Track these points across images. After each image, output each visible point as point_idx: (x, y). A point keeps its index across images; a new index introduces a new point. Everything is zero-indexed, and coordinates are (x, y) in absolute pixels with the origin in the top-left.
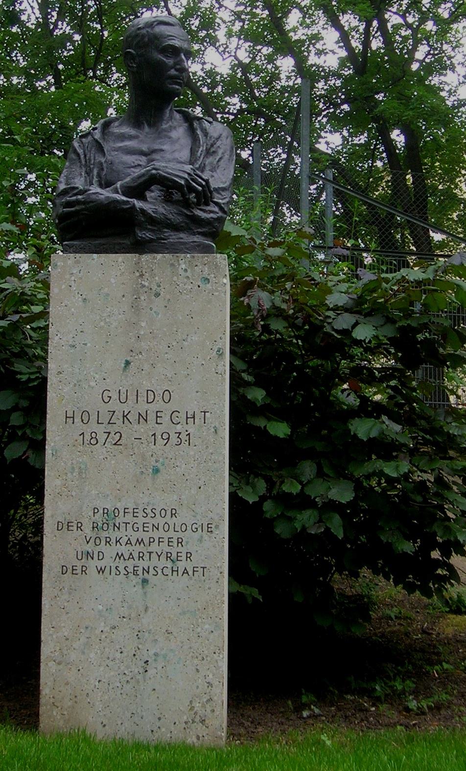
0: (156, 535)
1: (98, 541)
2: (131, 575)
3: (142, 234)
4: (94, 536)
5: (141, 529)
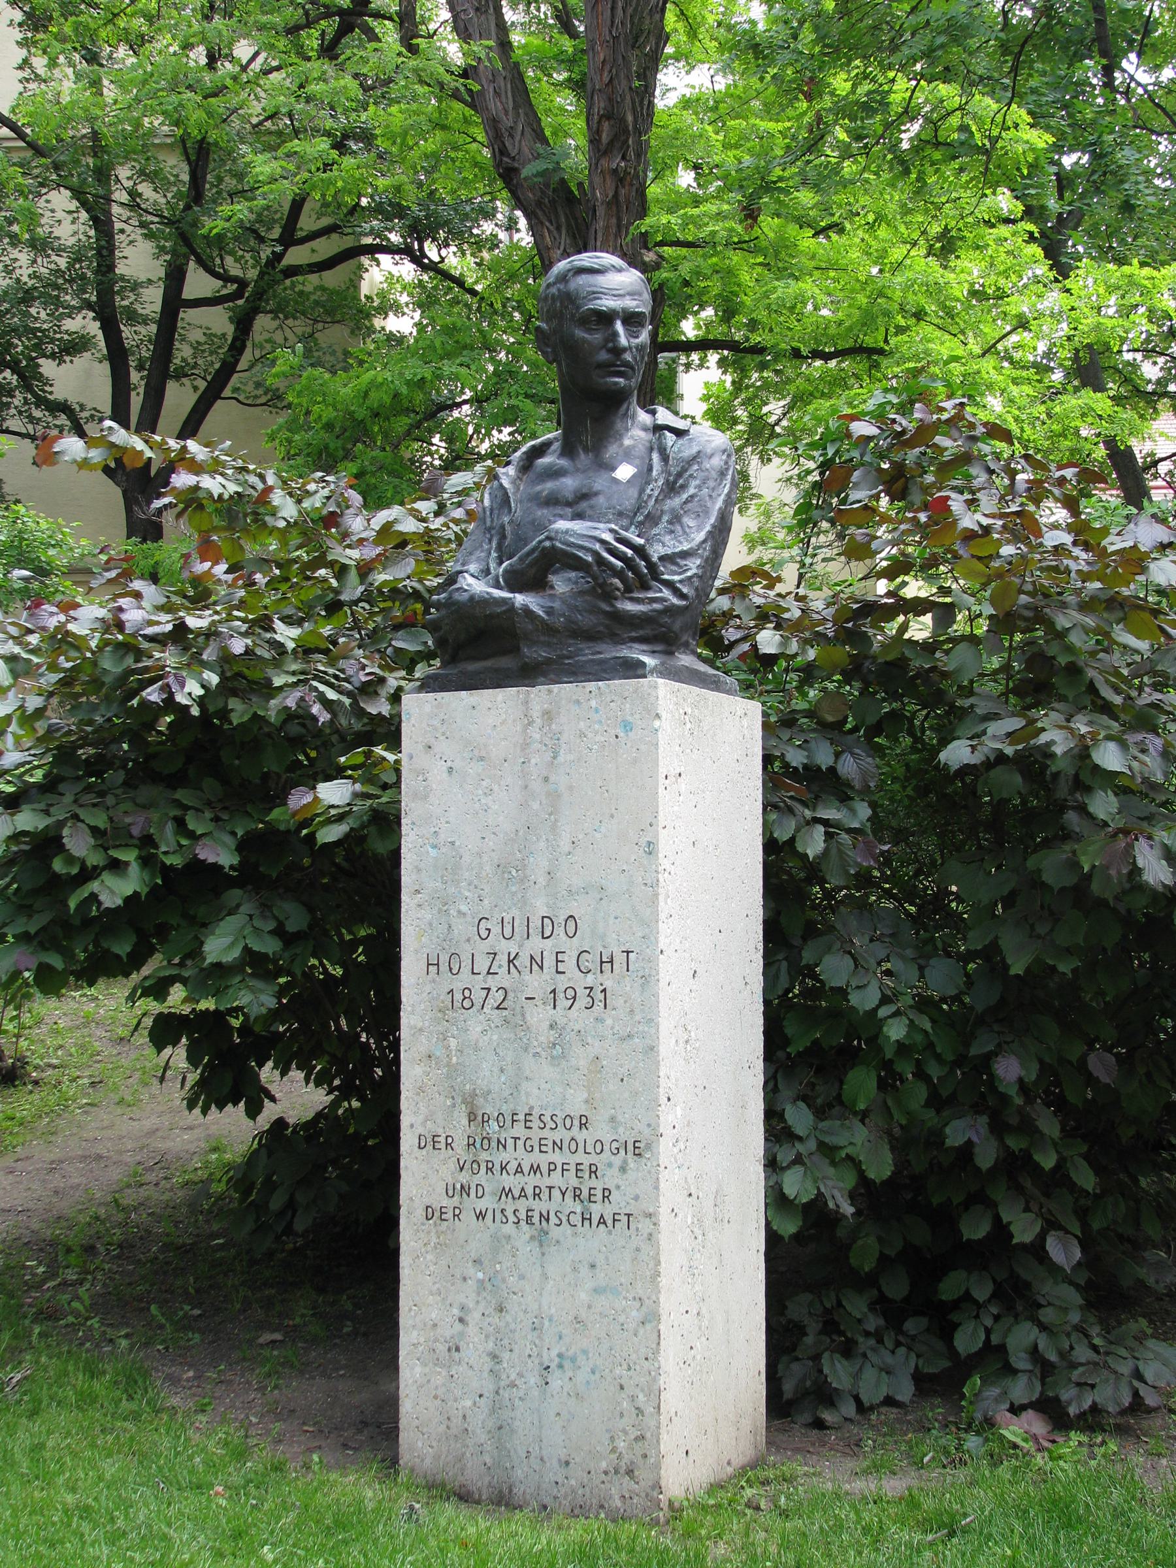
0: (558, 1158)
1: (475, 1166)
2: (523, 1223)
3: (534, 653)
4: (471, 1158)
5: (536, 1149)
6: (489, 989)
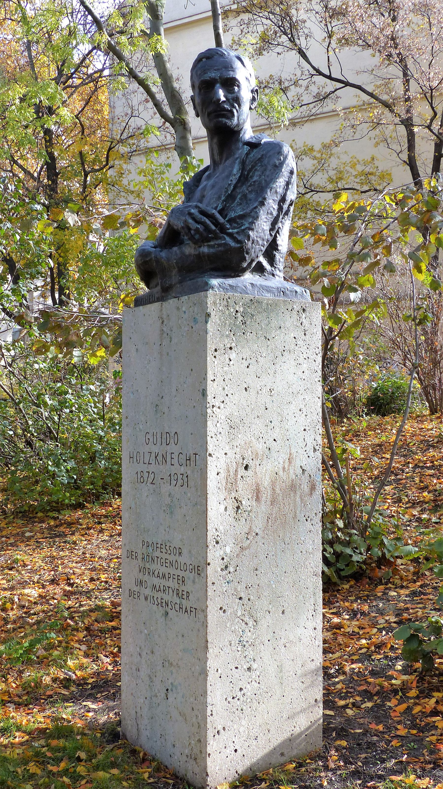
2: (160, 605)
6: (152, 483)
